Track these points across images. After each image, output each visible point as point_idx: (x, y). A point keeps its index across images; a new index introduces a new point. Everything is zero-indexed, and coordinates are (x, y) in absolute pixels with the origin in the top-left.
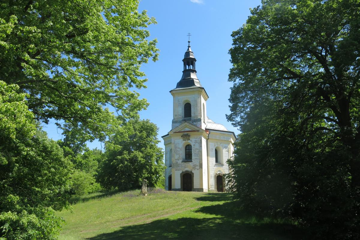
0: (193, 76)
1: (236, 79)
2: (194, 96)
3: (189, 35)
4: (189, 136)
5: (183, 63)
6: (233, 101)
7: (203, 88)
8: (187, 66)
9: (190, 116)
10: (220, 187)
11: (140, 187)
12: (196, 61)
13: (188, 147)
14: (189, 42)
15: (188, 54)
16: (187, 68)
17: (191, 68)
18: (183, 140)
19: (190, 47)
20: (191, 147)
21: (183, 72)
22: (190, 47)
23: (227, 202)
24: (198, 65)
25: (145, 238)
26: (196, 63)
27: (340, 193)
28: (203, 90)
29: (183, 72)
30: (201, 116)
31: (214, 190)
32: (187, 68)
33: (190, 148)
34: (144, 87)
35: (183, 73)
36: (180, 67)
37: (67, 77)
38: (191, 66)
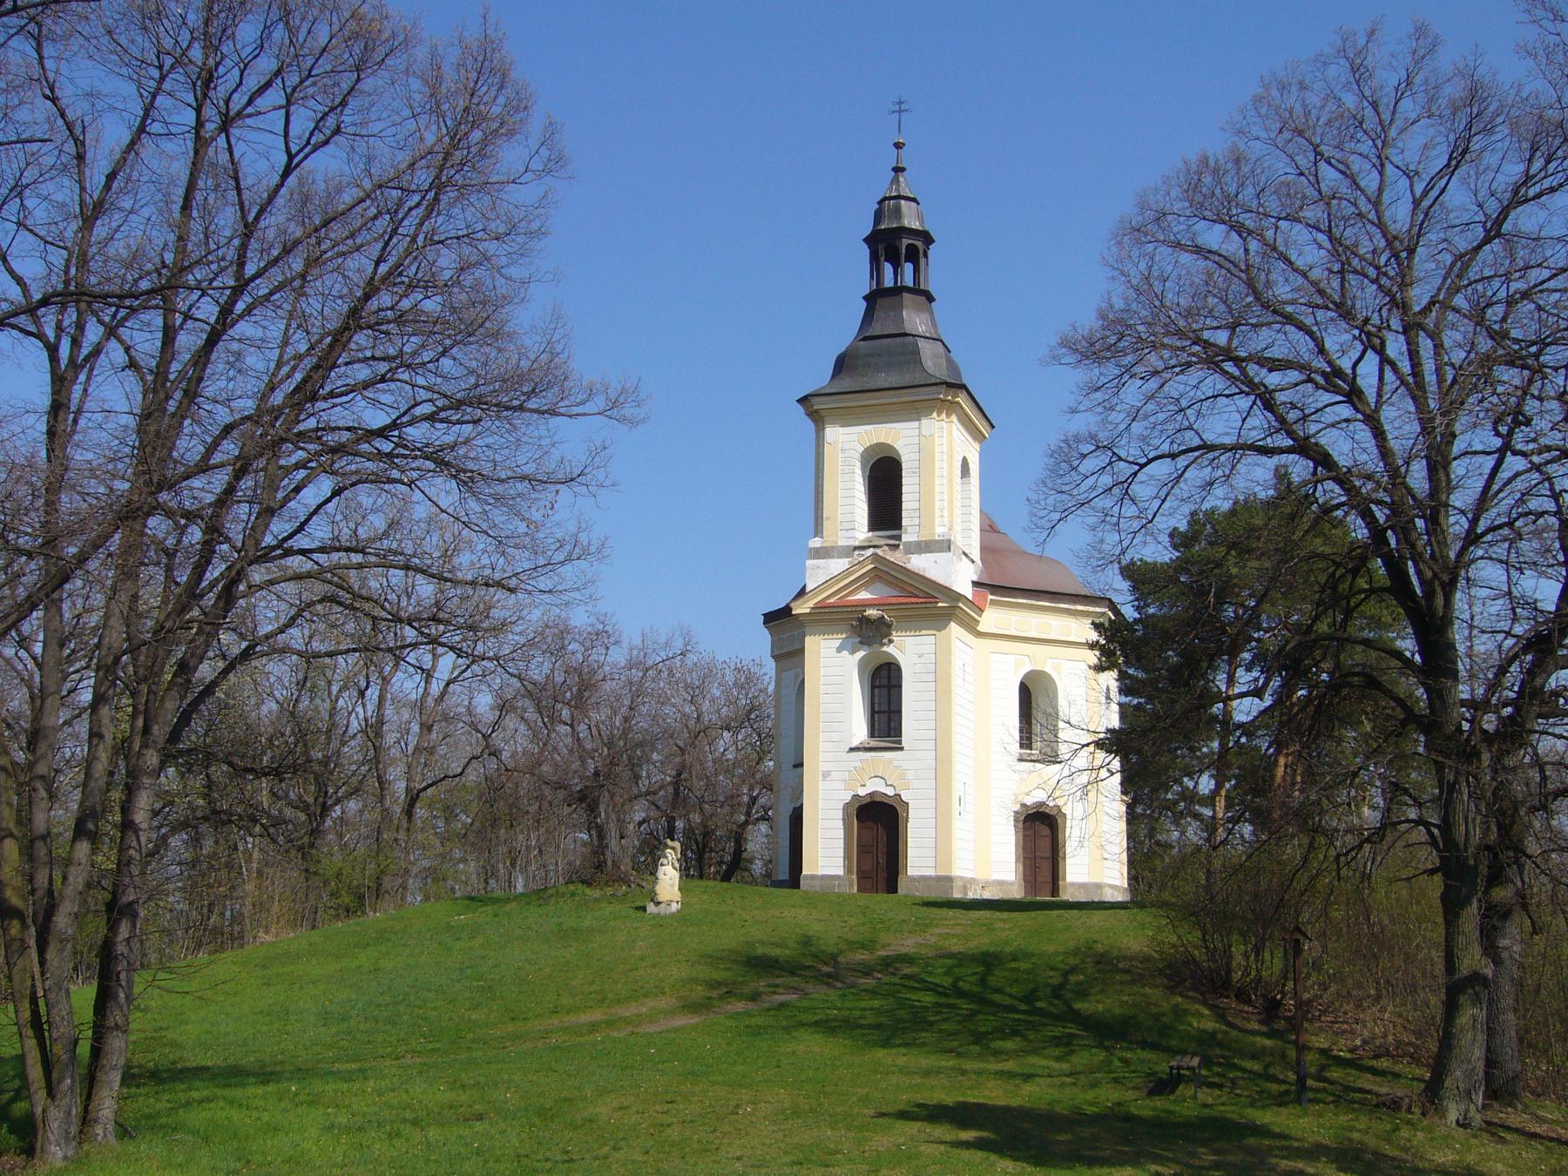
0: (915, 321)
1: (746, 823)
2: (916, 424)
3: (900, 109)
4: (889, 626)
7: (963, 387)
8: (888, 269)
9: (897, 524)
13: (884, 673)
14: (898, 146)
15: (887, 206)
16: (888, 282)
18: (861, 643)
19: (903, 170)
21: (864, 298)
22: (903, 170)
23: (1301, 1172)
24: (938, 270)
29: (864, 298)
31: (1012, 884)
32: (888, 282)
33: (893, 682)
35: (865, 304)
36: (856, 275)
37: (1339, 741)
38: (908, 268)
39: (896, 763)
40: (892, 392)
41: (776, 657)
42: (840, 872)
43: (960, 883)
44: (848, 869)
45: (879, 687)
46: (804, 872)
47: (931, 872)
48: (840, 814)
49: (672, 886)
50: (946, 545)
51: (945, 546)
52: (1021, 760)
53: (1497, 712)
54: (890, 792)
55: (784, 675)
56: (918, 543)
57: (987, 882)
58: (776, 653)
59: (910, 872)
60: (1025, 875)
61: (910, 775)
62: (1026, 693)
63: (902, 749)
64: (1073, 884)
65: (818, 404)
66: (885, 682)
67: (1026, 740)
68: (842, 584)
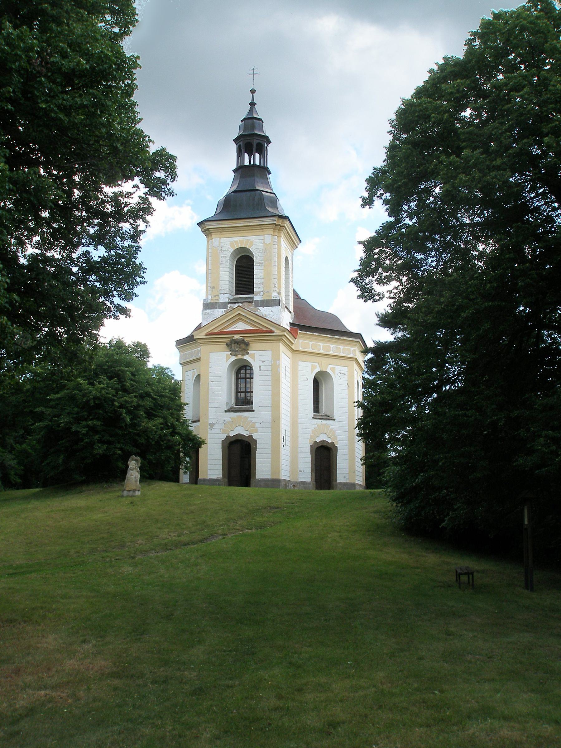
2: (262, 237)
4: (247, 344)
5: (234, 147)
6: (93, 14)
7: (287, 218)
8: (246, 156)
9: (250, 290)
10: (262, 484)
11: (176, 479)
12: (269, 142)
14: (253, 91)
17: (257, 163)
18: (231, 354)
20: (252, 374)
25: (526, 522)
26: (271, 149)
27: (354, 722)
28: (288, 222)
30: (279, 293)
31: (309, 483)
32: (247, 163)
33: (248, 376)
34: (132, 198)
39: (249, 419)
40: (224, 222)
41: (183, 364)
42: (220, 476)
43: (283, 483)
44: (223, 475)
45: (241, 378)
46: (200, 478)
47: (269, 477)
48: (220, 446)
49: (136, 481)
50: (277, 302)
51: (277, 303)
52: (313, 418)
53: (436, 197)
54: (330, 441)
55: (187, 373)
56: (262, 301)
57: (297, 483)
58: (183, 361)
59: (257, 478)
60: (316, 479)
61: (257, 425)
62: (317, 383)
63: (253, 411)
64: (340, 483)
65: (209, 225)
66: (243, 376)
67: (317, 409)
68: (221, 323)
